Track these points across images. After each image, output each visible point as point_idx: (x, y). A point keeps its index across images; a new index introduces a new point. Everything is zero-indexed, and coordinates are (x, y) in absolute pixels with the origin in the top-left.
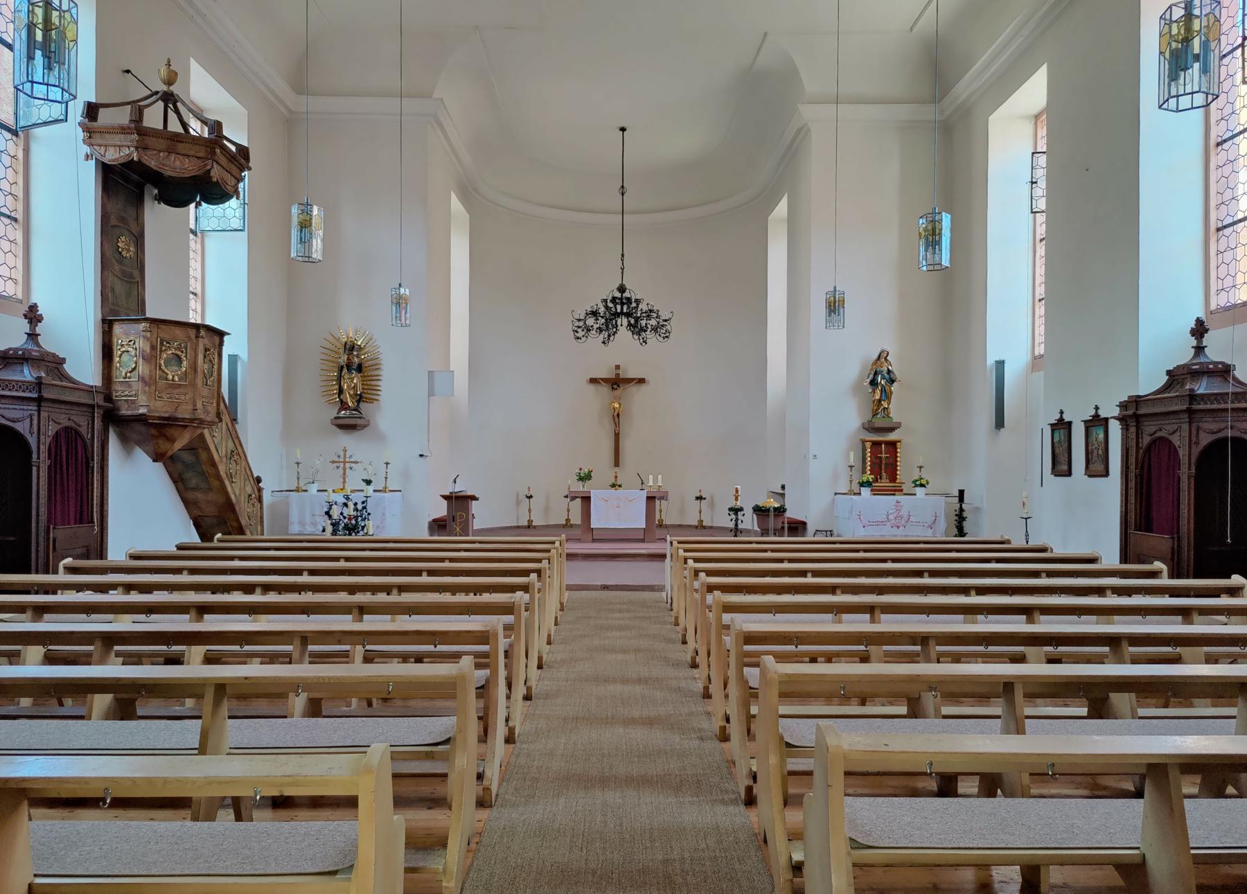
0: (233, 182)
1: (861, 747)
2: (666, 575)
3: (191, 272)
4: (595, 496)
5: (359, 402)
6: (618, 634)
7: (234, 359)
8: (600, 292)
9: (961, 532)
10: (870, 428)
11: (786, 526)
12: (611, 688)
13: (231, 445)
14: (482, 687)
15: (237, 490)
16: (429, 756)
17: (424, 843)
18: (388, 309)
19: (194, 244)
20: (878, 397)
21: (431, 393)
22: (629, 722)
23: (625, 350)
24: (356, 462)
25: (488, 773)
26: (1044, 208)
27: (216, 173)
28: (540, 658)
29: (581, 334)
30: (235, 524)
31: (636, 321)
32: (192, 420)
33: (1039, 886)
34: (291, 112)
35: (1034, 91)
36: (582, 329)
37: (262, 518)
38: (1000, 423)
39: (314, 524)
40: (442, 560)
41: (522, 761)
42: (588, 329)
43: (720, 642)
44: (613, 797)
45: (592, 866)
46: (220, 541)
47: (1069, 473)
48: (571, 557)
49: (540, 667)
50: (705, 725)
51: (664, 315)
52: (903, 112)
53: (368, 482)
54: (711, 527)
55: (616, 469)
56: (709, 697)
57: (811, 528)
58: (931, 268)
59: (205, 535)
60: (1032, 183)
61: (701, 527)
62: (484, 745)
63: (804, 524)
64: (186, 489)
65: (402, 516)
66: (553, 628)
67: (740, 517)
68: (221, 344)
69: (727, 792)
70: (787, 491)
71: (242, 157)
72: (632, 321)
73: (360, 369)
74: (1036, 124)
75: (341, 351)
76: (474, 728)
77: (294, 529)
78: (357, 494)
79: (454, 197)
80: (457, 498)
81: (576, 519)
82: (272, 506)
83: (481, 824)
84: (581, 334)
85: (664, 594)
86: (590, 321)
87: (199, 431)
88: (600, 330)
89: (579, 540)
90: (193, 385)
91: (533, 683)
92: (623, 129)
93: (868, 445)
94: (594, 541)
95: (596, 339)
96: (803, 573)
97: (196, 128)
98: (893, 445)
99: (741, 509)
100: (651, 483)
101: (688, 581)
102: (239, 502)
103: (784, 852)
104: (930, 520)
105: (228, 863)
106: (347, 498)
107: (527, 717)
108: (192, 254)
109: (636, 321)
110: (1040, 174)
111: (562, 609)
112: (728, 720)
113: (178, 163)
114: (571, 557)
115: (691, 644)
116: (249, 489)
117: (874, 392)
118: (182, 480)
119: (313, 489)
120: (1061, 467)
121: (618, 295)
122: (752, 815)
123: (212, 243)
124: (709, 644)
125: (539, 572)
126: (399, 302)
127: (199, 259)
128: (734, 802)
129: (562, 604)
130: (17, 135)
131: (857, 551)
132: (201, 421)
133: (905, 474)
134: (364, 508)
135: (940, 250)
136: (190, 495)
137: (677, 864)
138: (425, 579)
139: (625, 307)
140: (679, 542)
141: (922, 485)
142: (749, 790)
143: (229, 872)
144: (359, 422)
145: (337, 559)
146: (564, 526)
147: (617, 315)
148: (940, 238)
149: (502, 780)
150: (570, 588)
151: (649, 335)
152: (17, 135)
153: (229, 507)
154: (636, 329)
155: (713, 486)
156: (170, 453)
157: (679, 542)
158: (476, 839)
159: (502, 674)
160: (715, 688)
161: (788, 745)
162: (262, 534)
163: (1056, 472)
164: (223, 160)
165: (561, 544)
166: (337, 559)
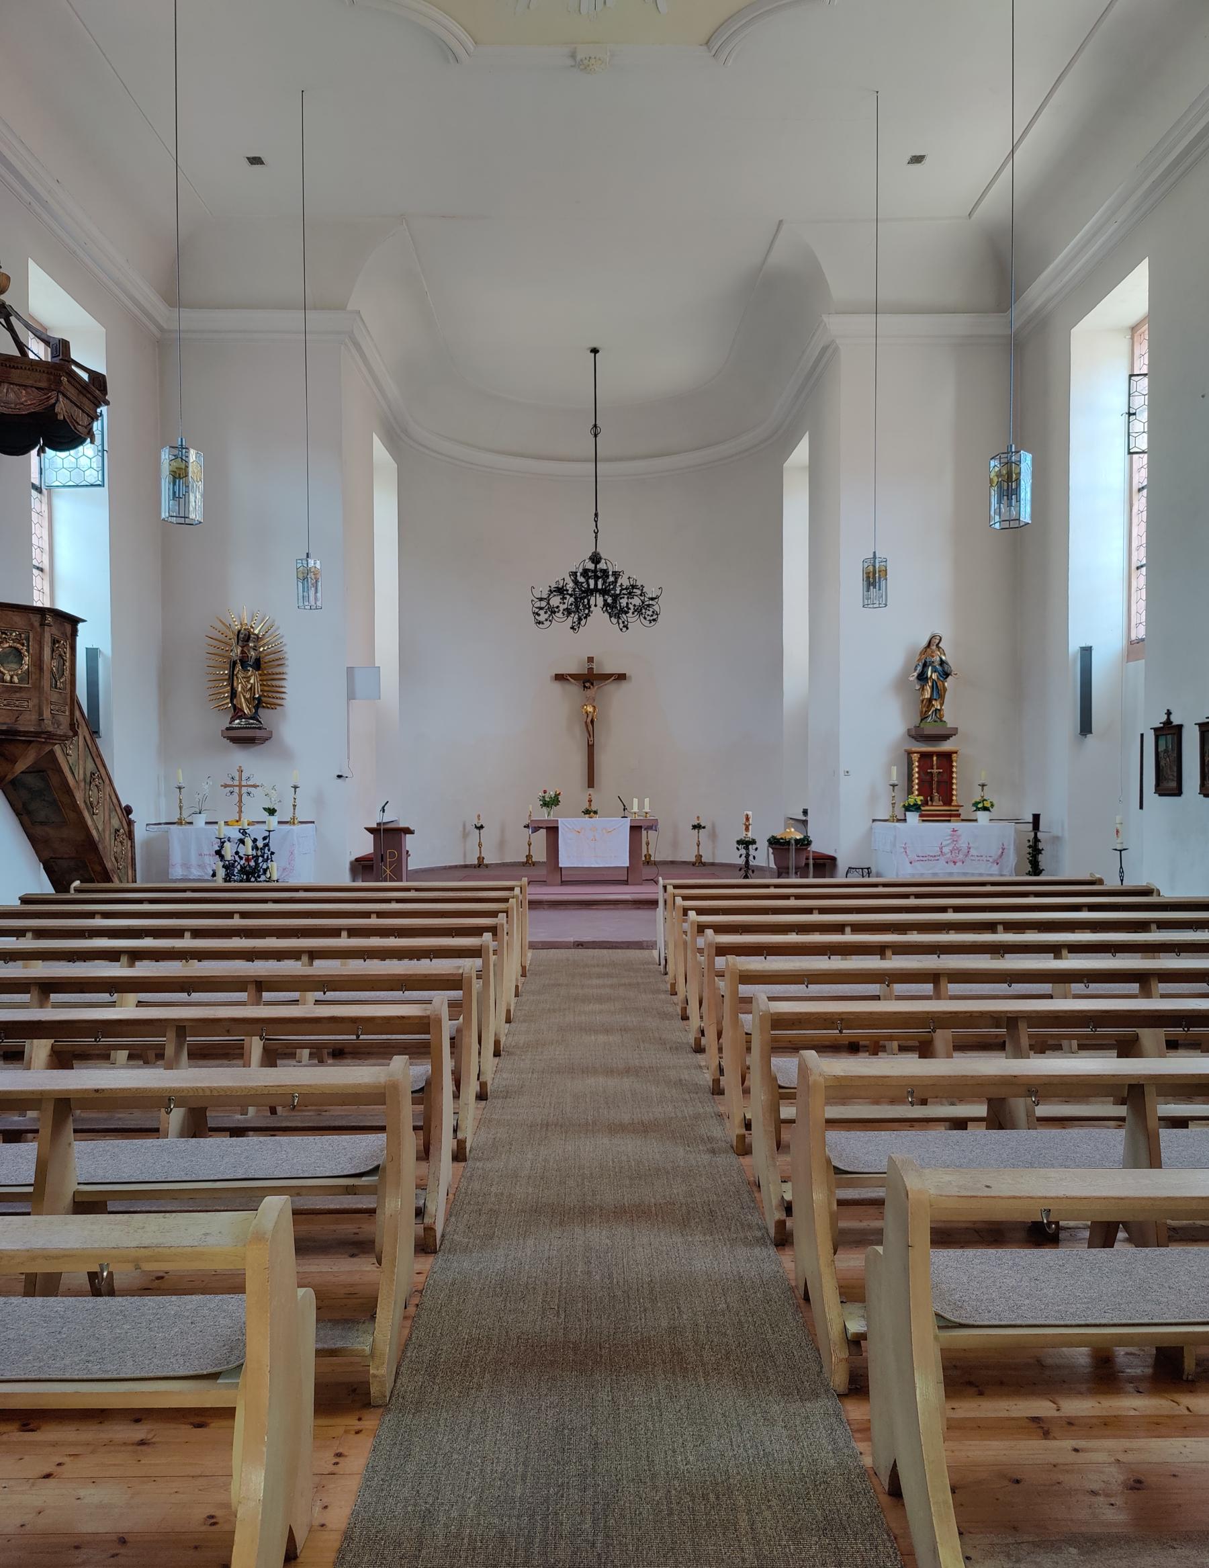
0: (86, 420)
1: (954, 1191)
2: (659, 928)
3: (35, 540)
4: (564, 825)
5: (257, 707)
6: (597, 1007)
7: (92, 654)
8: (565, 563)
9: (1036, 869)
10: (917, 735)
11: (811, 862)
12: (591, 1081)
13: (90, 766)
14: (422, 1090)
15: (99, 824)
16: (350, 1190)
17: (345, 1310)
18: (292, 586)
19: (37, 503)
20: (927, 695)
21: (351, 696)
22: (616, 1129)
23: (598, 639)
24: (255, 786)
25: (431, 1208)
26: (1144, 447)
27: (62, 408)
28: (497, 1043)
29: (543, 617)
30: (98, 868)
31: (615, 601)
32: (37, 734)
33: (1182, 1363)
34: (161, 329)
35: (1132, 295)
36: (544, 611)
37: (133, 859)
38: (1086, 727)
39: (202, 866)
40: (367, 915)
41: (476, 1186)
42: (553, 611)
43: (736, 1022)
44: (597, 1236)
45: (573, 1337)
46: (77, 890)
47: (1178, 792)
48: (534, 904)
49: (497, 1054)
50: (717, 1132)
51: (651, 591)
52: (960, 324)
53: (272, 812)
54: (713, 864)
55: (591, 791)
56: (721, 1093)
57: (842, 866)
58: (1006, 525)
59: (60, 884)
60: (1130, 414)
61: (699, 863)
62: (424, 1164)
63: (833, 859)
64: (34, 823)
65: (317, 856)
66: (513, 1000)
67: (752, 852)
68: (74, 633)
69: (750, 1227)
70: (810, 818)
71: (96, 389)
72: (610, 600)
73: (257, 665)
74: (1132, 338)
75: (234, 642)
76: (410, 1143)
77: (177, 872)
78: (257, 826)
79: (376, 439)
80: (386, 830)
81: (540, 855)
82: (148, 843)
83: (422, 1278)
84: (543, 617)
85: (655, 953)
86: (555, 601)
87: (47, 749)
88: (568, 612)
89: (543, 883)
90: (38, 688)
91: (488, 1077)
92: (595, 351)
93: (915, 757)
94: (563, 883)
95: (562, 624)
96: (839, 928)
97: (38, 351)
98: (947, 757)
99: (753, 842)
100: (635, 809)
101: (688, 938)
102: (102, 839)
103: (838, 1320)
104: (995, 852)
105: (67, 1361)
106: (244, 832)
107: (481, 1123)
108: (34, 516)
109: (615, 601)
110: (1140, 402)
111: (524, 975)
112: (748, 1126)
113: (12, 395)
114: (534, 904)
115: (695, 1022)
116: (115, 823)
117: (923, 688)
118: (29, 813)
119: (200, 821)
120: (1168, 782)
121: (591, 566)
122: (786, 1260)
123: (65, 507)
124: (719, 1023)
125: (493, 930)
126: (307, 578)
127: (46, 524)
128: (760, 1241)
129: (524, 968)
130: (41, 492)
131: (906, 896)
132: (50, 736)
133: (963, 793)
134: (267, 845)
135: (1018, 501)
136: (39, 831)
137: (689, 1334)
138: (344, 942)
139: (600, 582)
140: (675, 887)
141: (985, 809)
142: (781, 1225)
143: (67, 1376)
144: (258, 733)
145: (229, 915)
146: (524, 864)
147: (590, 592)
148: (1018, 485)
149: (449, 1215)
150: (533, 946)
151: (631, 617)
152: (41, 492)
153: (90, 846)
154: (615, 610)
155: (730, 815)
156: (10, 777)
157: (675, 887)
158: (416, 1300)
159: (448, 1064)
160: (730, 1082)
161: (838, 1171)
162: (134, 881)
163: (1161, 790)
164: (72, 392)
165: (522, 889)
166: (229, 915)
